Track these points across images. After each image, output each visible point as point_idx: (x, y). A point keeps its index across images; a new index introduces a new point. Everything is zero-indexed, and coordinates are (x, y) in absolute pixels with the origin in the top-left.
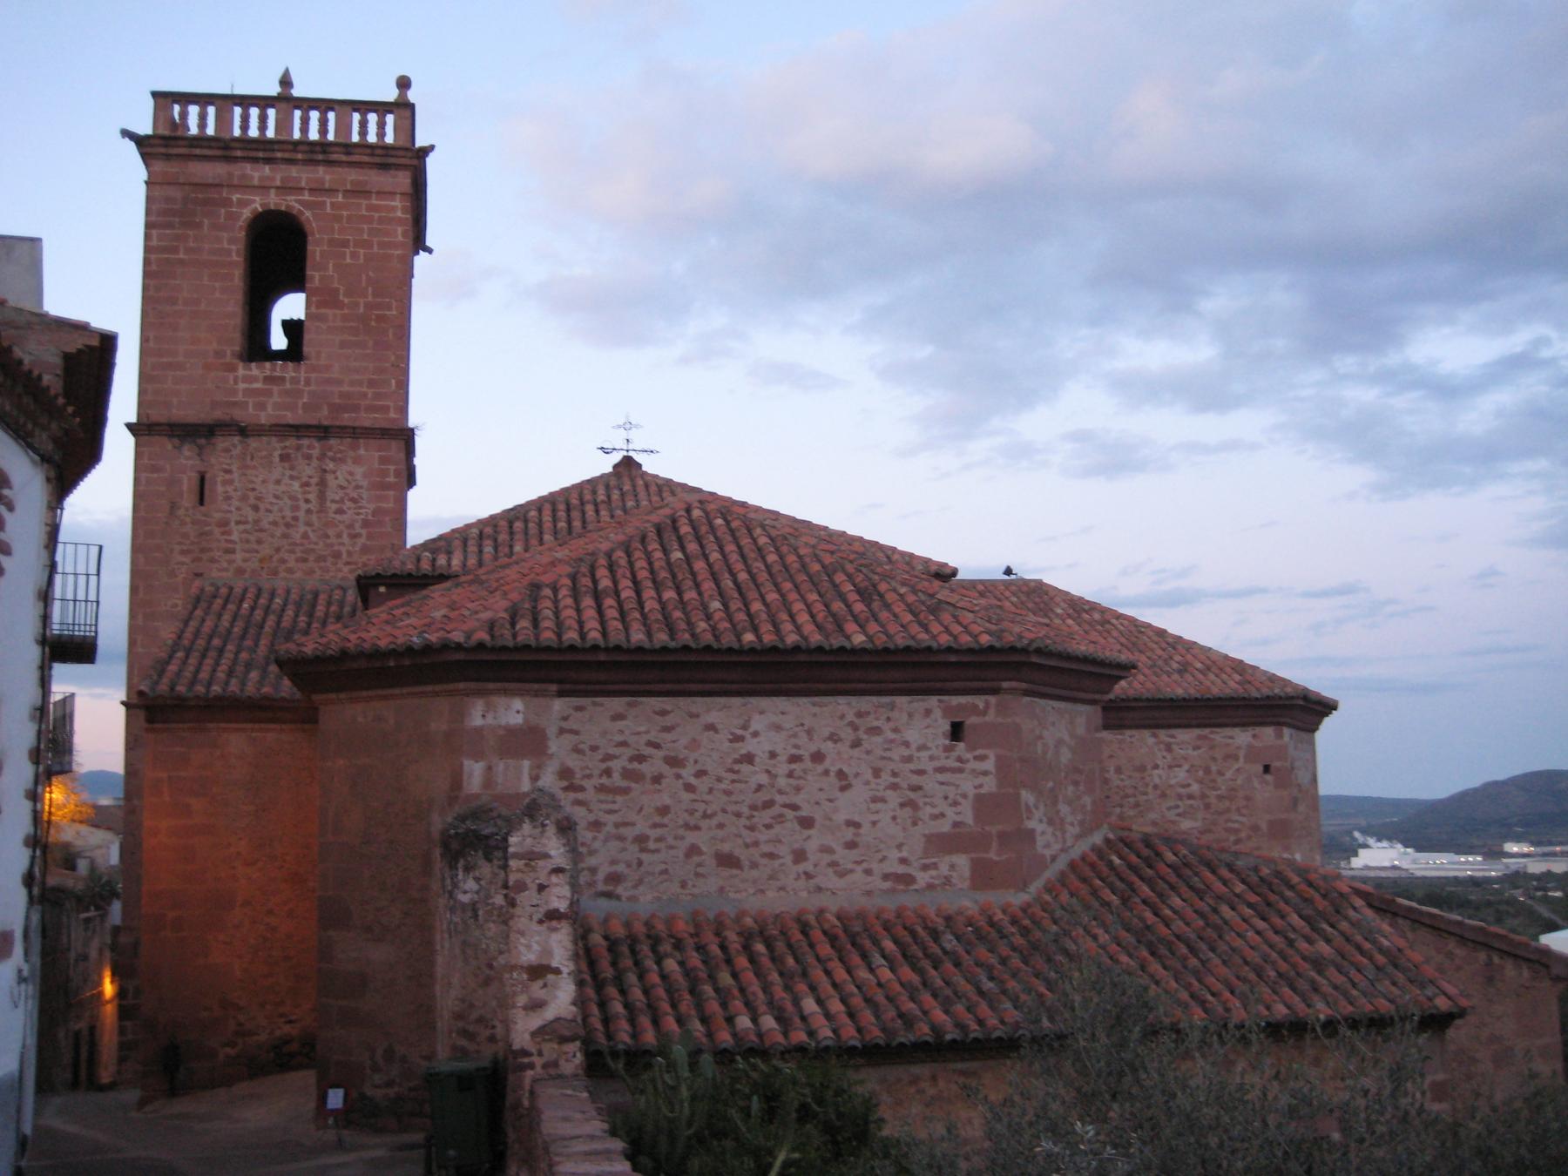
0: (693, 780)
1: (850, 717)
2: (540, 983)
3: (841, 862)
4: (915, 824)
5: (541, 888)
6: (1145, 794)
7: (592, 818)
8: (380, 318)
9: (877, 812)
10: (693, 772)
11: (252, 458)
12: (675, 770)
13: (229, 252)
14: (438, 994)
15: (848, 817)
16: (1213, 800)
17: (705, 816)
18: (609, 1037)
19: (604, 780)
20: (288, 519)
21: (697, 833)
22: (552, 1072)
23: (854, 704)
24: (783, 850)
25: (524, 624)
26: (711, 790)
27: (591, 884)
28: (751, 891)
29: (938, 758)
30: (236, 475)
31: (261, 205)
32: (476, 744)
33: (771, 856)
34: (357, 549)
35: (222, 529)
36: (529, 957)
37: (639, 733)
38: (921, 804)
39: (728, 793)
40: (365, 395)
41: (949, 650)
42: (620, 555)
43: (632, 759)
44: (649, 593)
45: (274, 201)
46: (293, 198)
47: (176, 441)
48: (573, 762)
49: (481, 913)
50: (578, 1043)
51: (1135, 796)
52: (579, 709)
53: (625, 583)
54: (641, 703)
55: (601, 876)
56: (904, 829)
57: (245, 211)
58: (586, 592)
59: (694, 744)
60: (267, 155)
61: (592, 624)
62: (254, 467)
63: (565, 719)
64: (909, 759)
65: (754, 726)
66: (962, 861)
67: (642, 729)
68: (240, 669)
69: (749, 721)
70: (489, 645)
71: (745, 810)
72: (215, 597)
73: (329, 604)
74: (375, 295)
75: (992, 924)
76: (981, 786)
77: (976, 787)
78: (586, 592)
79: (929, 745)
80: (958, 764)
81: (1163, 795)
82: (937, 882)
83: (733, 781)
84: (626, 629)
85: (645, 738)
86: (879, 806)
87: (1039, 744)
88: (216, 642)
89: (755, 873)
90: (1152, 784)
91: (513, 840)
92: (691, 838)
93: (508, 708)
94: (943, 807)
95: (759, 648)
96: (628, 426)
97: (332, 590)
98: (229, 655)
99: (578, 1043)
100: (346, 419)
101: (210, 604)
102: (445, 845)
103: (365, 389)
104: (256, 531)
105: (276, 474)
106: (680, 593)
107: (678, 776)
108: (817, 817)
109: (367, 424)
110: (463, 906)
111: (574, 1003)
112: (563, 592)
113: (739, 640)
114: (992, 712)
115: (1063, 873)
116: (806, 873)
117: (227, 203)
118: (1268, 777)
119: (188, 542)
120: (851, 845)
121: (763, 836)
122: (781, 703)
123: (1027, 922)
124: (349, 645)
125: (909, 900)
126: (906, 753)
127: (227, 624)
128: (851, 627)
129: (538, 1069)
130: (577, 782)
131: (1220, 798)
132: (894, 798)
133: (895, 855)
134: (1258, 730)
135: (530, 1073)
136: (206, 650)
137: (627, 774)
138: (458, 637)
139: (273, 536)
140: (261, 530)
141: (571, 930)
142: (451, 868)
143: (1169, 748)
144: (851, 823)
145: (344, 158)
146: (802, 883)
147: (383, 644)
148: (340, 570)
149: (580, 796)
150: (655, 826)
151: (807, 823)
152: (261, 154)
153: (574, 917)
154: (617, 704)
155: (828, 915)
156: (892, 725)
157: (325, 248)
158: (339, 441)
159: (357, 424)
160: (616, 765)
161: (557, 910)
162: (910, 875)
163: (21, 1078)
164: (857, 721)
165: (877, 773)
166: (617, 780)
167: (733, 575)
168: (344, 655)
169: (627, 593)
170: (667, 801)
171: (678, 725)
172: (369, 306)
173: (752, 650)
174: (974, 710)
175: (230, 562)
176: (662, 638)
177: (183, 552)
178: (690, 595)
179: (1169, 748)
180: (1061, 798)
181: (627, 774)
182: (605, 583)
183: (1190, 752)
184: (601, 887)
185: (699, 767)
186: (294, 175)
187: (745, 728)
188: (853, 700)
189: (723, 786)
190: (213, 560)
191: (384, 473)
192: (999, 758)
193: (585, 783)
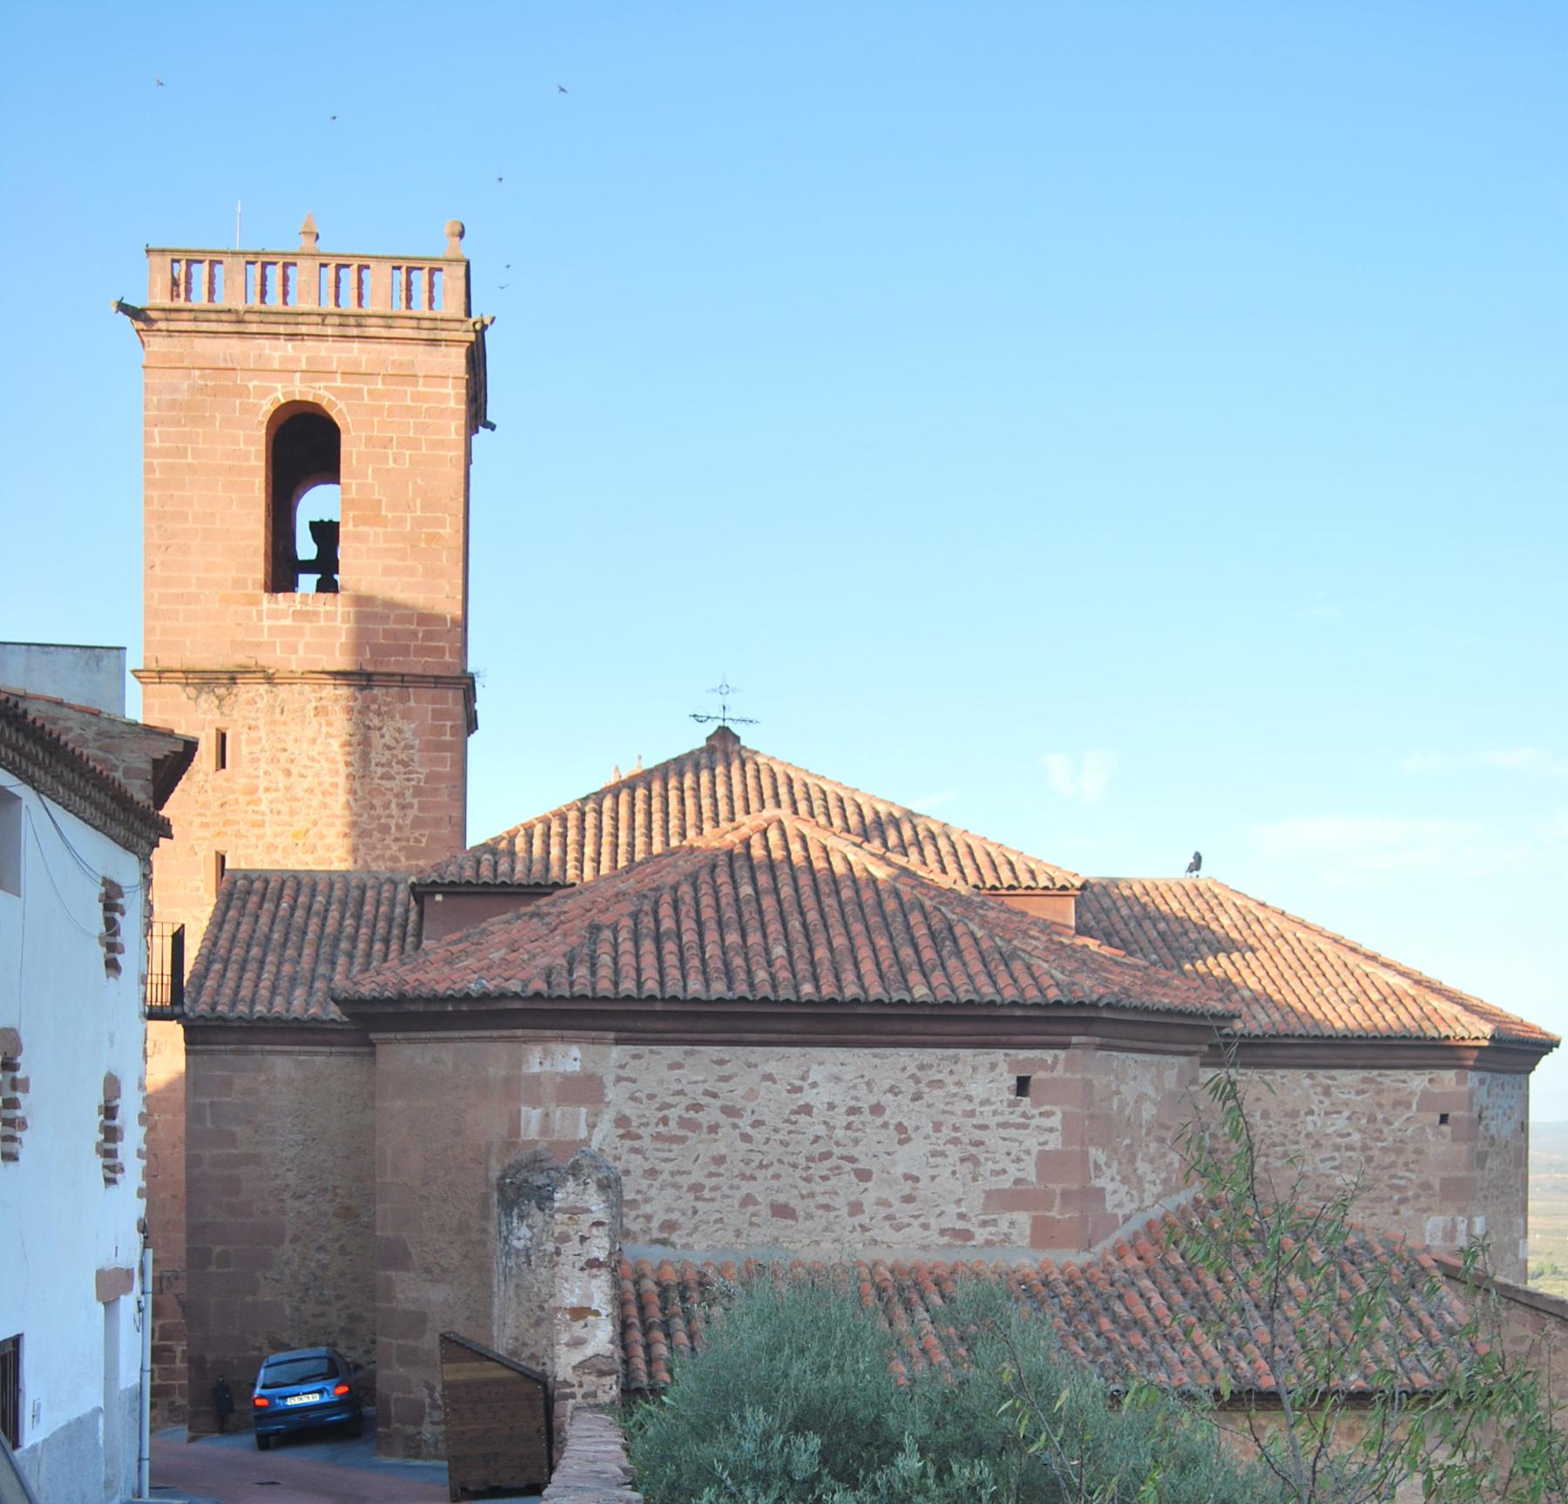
0: (749, 1130)
1: (912, 1069)
2: (582, 1323)
3: (898, 1216)
4: (975, 1179)
5: (583, 1239)
6: (1297, 1143)
7: (648, 1166)
8: (432, 538)
9: (937, 1166)
10: (750, 1122)
11: (282, 712)
12: (731, 1120)
13: (246, 456)
14: (495, 1334)
15: (905, 1171)
17: (761, 1166)
18: (650, 1375)
19: (661, 1129)
20: (326, 786)
21: (752, 1183)
22: (591, 1401)
23: (916, 1056)
24: (840, 1202)
25: (582, 971)
26: (768, 1140)
29: (1002, 1113)
30: (263, 733)
31: (284, 394)
32: (532, 1090)
33: (827, 1208)
34: (408, 822)
35: (248, 798)
36: (572, 1300)
37: (695, 1082)
38: (982, 1160)
39: (784, 1144)
40: (415, 634)
41: (1014, 1004)
42: (686, 890)
43: (688, 1109)
44: (712, 936)
45: (301, 390)
47: (191, 691)
48: (630, 1110)
49: (533, 1258)
50: (614, 1377)
51: (1283, 1144)
52: (637, 1057)
53: (688, 924)
54: (699, 1052)
55: (655, 1223)
56: (964, 1184)
57: (264, 402)
58: (647, 935)
59: (752, 1094)
60: (291, 329)
61: (650, 973)
62: (285, 723)
63: (622, 1067)
65: (813, 1077)
66: (1023, 1219)
67: (700, 1078)
68: (284, 984)
69: (808, 1071)
70: (546, 995)
71: (802, 1162)
72: (249, 893)
73: (378, 903)
74: (422, 508)
75: (1046, 1284)
76: (1045, 1143)
77: (1040, 1144)
78: (647, 935)
79: (993, 1099)
80: (1022, 1120)
81: (1317, 1145)
82: (995, 1239)
83: (790, 1132)
84: (684, 977)
85: (703, 1087)
86: (939, 1160)
87: (1116, 1099)
88: (255, 951)
89: (809, 1223)
90: (1304, 1133)
91: (557, 1196)
92: (746, 1187)
93: (566, 1055)
94: (1005, 1162)
95: (816, 999)
96: (724, 690)
97: (381, 885)
98: (270, 968)
99: (614, 1377)
100: (393, 664)
101: (245, 903)
102: (501, 1188)
103: (414, 627)
104: (288, 800)
105: (310, 733)
106: (744, 936)
107: (735, 1126)
109: (418, 670)
110: (518, 1251)
111: (612, 1342)
112: (624, 935)
114: (1060, 1067)
115: (1136, 1234)
116: (861, 1226)
117: (243, 392)
118: (1445, 1128)
119: (208, 813)
120: (909, 1199)
121: (819, 1187)
122: (840, 1053)
123: (1082, 1283)
124: (407, 987)
125: (966, 1255)
126: (970, 1107)
127: (266, 929)
128: (914, 977)
129: (579, 1399)
130: (633, 1130)
131: (1385, 1150)
132: (954, 1153)
134: (1436, 1073)
135: (571, 1401)
136: (245, 961)
137: (683, 1123)
138: (514, 986)
139: (309, 807)
140: (296, 799)
141: (609, 1277)
142: (506, 1215)
143: (1327, 1092)
144: (907, 1177)
145: (384, 332)
146: (857, 1235)
147: (440, 989)
148: (388, 847)
149: (636, 1144)
150: (711, 1175)
151: (864, 1175)
152: (282, 329)
153: (614, 1265)
154: (674, 1052)
155: (881, 1269)
156: (955, 1078)
157: (363, 449)
158: (384, 690)
159: (404, 670)
160: (673, 1114)
161: (597, 1259)
162: (968, 1231)
165: (937, 1127)
166: (673, 1128)
168: (402, 998)
169: (689, 937)
170: (724, 1151)
171: (736, 1074)
172: (417, 523)
173: (810, 1002)
174: (1042, 1064)
175: (259, 837)
176: (719, 988)
177: (204, 825)
178: (754, 938)
179: (1327, 1092)
180: (1140, 1156)
181: (683, 1123)
182: (667, 924)
183: (1353, 1096)
184: (656, 1234)
185: (754, 1117)
186: (323, 354)
187: (803, 1078)
188: (915, 1051)
189: (779, 1137)
190: (238, 835)
191: (439, 731)
192: (1065, 1115)
193: (641, 1131)
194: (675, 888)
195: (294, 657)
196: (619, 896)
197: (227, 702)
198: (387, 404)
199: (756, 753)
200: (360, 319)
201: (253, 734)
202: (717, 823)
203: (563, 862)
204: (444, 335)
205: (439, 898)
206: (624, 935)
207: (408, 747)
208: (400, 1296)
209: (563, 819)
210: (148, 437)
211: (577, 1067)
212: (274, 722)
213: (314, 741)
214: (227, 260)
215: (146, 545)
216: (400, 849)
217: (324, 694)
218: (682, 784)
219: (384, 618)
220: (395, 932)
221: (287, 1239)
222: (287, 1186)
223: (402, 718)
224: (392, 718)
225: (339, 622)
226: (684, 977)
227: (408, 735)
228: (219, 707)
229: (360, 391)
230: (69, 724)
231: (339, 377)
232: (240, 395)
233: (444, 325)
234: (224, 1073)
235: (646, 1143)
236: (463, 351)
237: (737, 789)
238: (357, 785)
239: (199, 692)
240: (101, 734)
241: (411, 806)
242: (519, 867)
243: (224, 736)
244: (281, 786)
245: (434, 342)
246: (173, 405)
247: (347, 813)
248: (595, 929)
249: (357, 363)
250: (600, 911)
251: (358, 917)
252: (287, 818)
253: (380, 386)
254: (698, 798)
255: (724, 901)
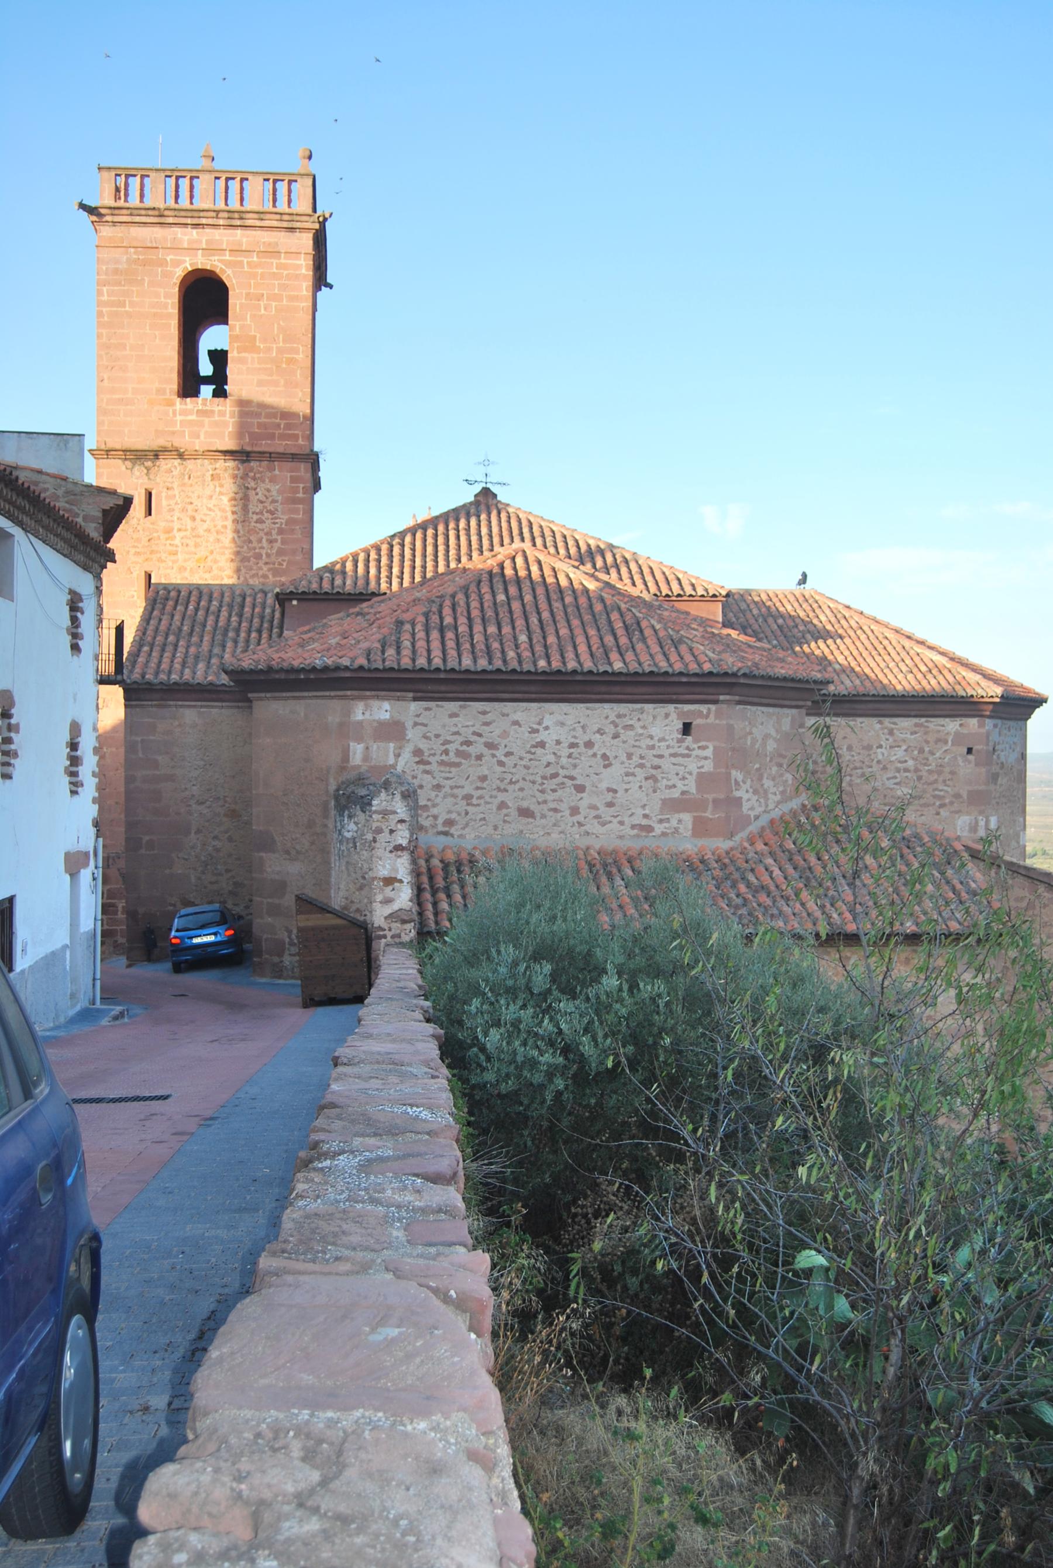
0: (503, 759)
1: (612, 717)
2: (391, 888)
4: (655, 791)
5: (392, 831)
6: (871, 767)
7: (435, 782)
8: (290, 361)
12: (491, 752)
13: (166, 306)
16: (924, 773)
17: (511, 782)
18: (437, 923)
19: (444, 757)
20: (219, 527)
22: (397, 940)
24: (564, 807)
25: (391, 652)
26: (516, 765)
27: (434, 826)
28: (542, 833)
29: (673, 747)
30: (176, 492)
32: (357, 731)
33: (555, 810)
34: (274, 551)
35: (167, 536)
36: (384, 873)
39: (527, 767)
40: (279, 425)
41: (681, 674)
42: (460, 598)
43: (462, 744)
44: (478, 628)
45: (202, 262)
46: (216, 258)
47: (128, 464)
48: (423, 745)
52: (428, 709)
53: (462, 620)
55: (440, 821)
59: (505, 734)
60: (196, 221)
61: (436, 653)
62: (191, 485)
63: (418, 716)
64: (653, 747)
65: (546, 723)
66: (687, 818)
72: (167, 599)
73: (254, 606)
74: (284, 341)
76: (702, 767)
80: (686, 752)
81: (885, 768)
83: (531, 760)
84: (460, 656)
85: (472, 729)
86: (631, 778)
88: (171, 638)
89: (543, 821)
91: (374, 802)
92: (501, 797)
93: (380, 708)
94: (675, 780)
96: (486, 463)
98: (181, 649)
100: (264, 446)
101: (164, 606)
102: (337, 798)
103: (278, 421)
106: (500, 629)
107: (494, 756)
108: (587, 784)
109: (281, 450)
112: (419, 627)
113: (535, 665)
114: (712, 716)
115: (763, 828)
116: (578, 823)
117: (163, 263)
118: (971, 757)
119: (140, 545)
120: (610, 805)
121: (550, 797)
122: (564, 707)
123: (727, 861)
125: (649, 842)
126: (651, 743)
127: (178, 623)
128: (614, 656)
129: (389, 938)
130: (425, 758)
131: (930, 772)
132: (641, 774)
133: (640, 812)
134: (964, 720)
135: (383, 941)
136: (165, 645)
137: (459, 753)
139: (207, 541)
140: (199, 537)
143: (891, 732)
144: (609, 790)
145: (258, 223)
147: (296, 663)
149: (427, 767)
150: (478, 788)
151: (580, 789)
152: (189, 221)
153: (412, 849)
154: (452, 706)
155: (592, 851)
156: (641, 723)
160: (452, 747)
161: (401, 845)
163: (95, 935)
164: (617, 721)
165: (629, 756)
166: (452, 757)
167: (539, 613)
168: (270, 669)
169: (463, 629)
170: (486, 772)
172: (280, 351)
173: (544, 673)
174: (700, 714)
175: (174, 562)
176: (483, 663)
177: (137, 554)
178: (506, 629)
179: (891, 732)
180: (765, 776)
181: (459, 753)
182: (448, 620)
183: (908, 736)
184: (440, 828)
185: (507, 750)
186: (217, 238)
187: (539, 724)
189: (523, 763)
190: (160, 560)
191: (295, 490)
192: (715, 748)
193: (430, 759)
194: (453, 596)
195: (197, 441)
196: (416, 601)
197: (153, 471)
198: (260, 271)
199: (508, 505)
200: (242, 214)
201: (170, 492)
202: (481, 552)
203: (378, 578)
204: (298, 225)
205: (295, 602)
206: (419, 627)
207: (274, 501)
208: (269, 870)
209: (378, 550)
210: (100, 293)
211: (387, 716)
212: (184, 485)
213: (211, 497)
214: (152, 174)
215: (98, 366)
216: (269, 570)
217: (217, 466)
218: (458, 526)
219: (258, 415)
220: (266, 625)
221: (193, 832)
222: (193, 796)
223: (270, 481)
224: (263, 481)
225: (227, 418)
226: (460, 656)
227: (274, 493)
228: (147, 474)
229: (242, 262)
230: (46, 486)
231: (227, 253)
232: (161, 265)
233: (298, 218)
234: (151, 720)
235: (434, 767)
236: (310, 235)
237: (495, 530)
238: (240, 527)
239: (134, 464)
240: (68, 493)
241: (276, 541)
242: (349, 582)
243: (150, 494)
244: (189, 527)
245: (292, 229)
246: (116, 271)
247: (233, 545)
248: (400, 623)
249: (240, 244)
250: (403, 612)
251: (240, 615)
252: (193, 549)
253: (255, 259)
254: (468, 535)
255: (486, 605)
